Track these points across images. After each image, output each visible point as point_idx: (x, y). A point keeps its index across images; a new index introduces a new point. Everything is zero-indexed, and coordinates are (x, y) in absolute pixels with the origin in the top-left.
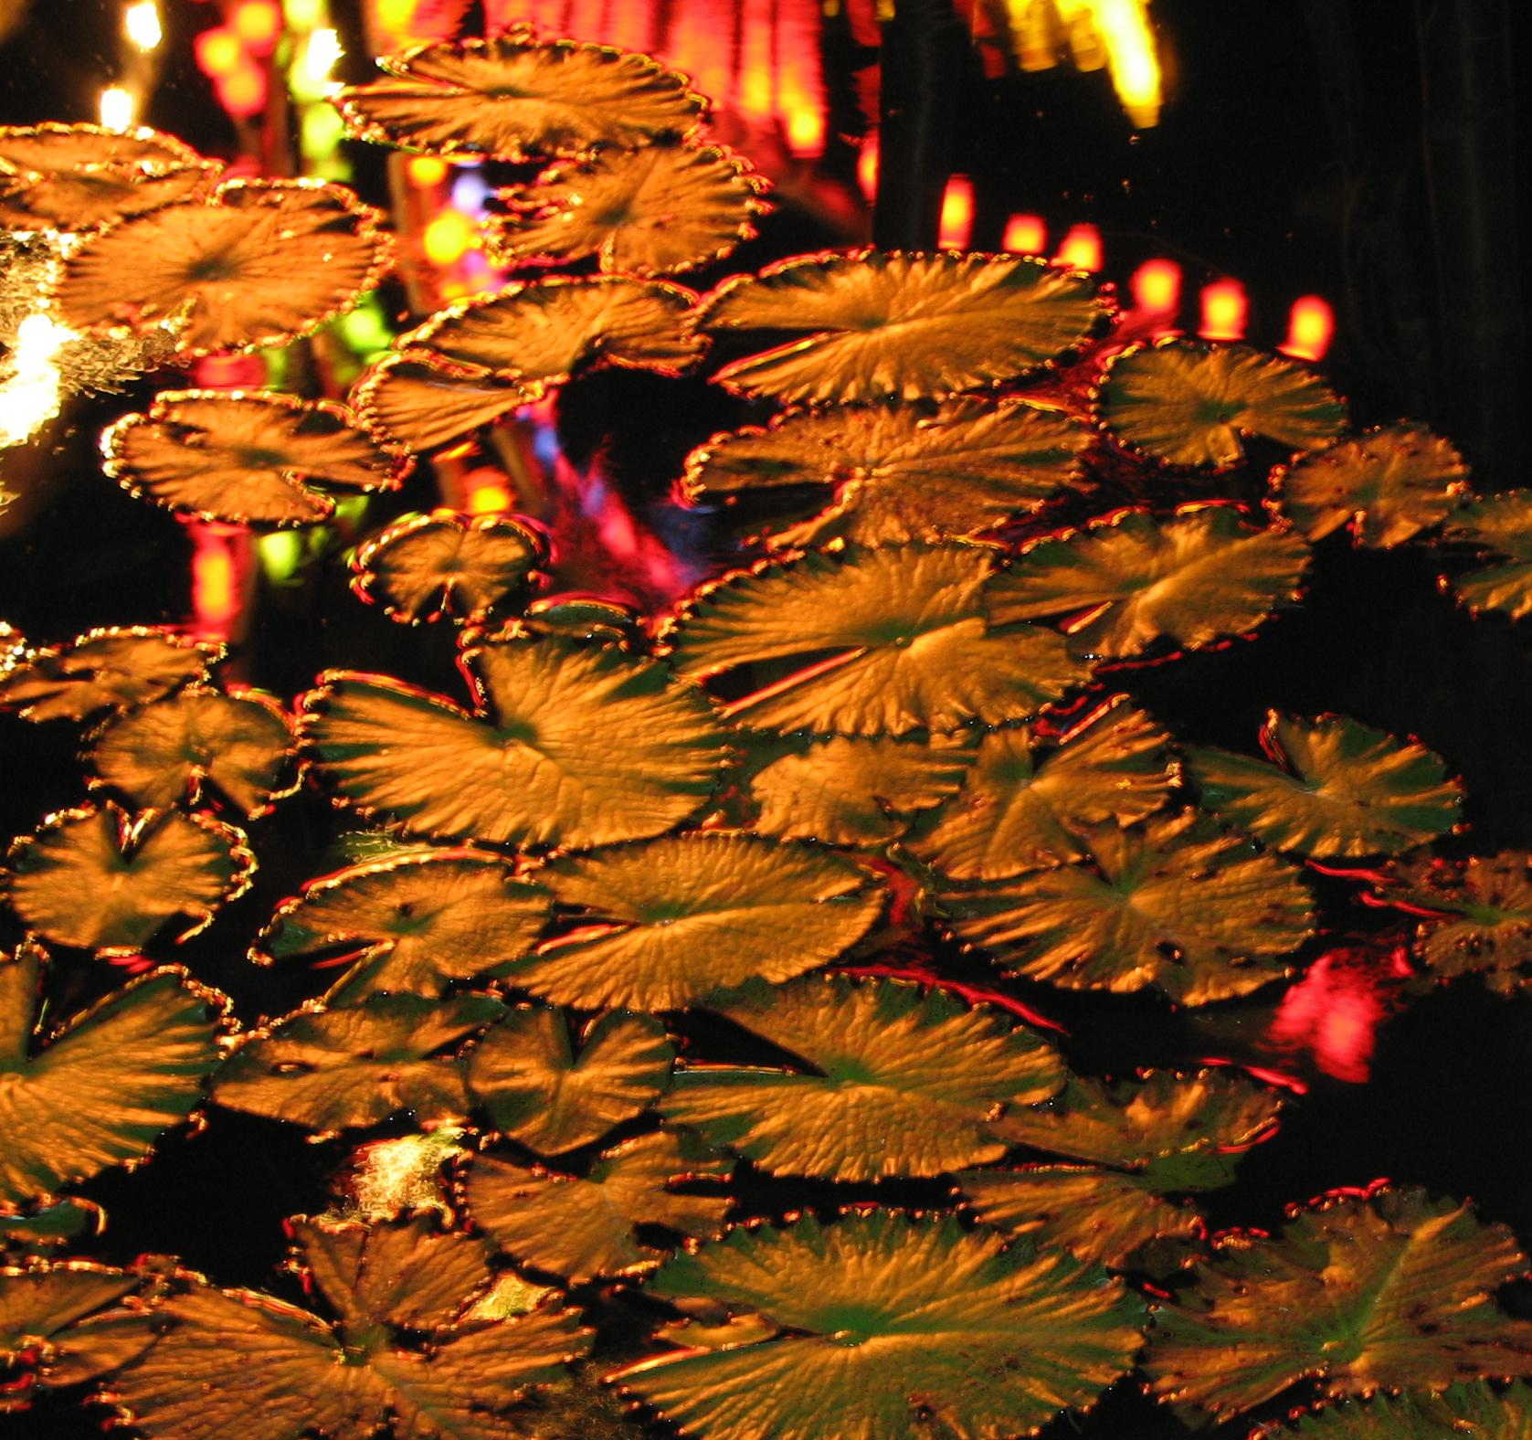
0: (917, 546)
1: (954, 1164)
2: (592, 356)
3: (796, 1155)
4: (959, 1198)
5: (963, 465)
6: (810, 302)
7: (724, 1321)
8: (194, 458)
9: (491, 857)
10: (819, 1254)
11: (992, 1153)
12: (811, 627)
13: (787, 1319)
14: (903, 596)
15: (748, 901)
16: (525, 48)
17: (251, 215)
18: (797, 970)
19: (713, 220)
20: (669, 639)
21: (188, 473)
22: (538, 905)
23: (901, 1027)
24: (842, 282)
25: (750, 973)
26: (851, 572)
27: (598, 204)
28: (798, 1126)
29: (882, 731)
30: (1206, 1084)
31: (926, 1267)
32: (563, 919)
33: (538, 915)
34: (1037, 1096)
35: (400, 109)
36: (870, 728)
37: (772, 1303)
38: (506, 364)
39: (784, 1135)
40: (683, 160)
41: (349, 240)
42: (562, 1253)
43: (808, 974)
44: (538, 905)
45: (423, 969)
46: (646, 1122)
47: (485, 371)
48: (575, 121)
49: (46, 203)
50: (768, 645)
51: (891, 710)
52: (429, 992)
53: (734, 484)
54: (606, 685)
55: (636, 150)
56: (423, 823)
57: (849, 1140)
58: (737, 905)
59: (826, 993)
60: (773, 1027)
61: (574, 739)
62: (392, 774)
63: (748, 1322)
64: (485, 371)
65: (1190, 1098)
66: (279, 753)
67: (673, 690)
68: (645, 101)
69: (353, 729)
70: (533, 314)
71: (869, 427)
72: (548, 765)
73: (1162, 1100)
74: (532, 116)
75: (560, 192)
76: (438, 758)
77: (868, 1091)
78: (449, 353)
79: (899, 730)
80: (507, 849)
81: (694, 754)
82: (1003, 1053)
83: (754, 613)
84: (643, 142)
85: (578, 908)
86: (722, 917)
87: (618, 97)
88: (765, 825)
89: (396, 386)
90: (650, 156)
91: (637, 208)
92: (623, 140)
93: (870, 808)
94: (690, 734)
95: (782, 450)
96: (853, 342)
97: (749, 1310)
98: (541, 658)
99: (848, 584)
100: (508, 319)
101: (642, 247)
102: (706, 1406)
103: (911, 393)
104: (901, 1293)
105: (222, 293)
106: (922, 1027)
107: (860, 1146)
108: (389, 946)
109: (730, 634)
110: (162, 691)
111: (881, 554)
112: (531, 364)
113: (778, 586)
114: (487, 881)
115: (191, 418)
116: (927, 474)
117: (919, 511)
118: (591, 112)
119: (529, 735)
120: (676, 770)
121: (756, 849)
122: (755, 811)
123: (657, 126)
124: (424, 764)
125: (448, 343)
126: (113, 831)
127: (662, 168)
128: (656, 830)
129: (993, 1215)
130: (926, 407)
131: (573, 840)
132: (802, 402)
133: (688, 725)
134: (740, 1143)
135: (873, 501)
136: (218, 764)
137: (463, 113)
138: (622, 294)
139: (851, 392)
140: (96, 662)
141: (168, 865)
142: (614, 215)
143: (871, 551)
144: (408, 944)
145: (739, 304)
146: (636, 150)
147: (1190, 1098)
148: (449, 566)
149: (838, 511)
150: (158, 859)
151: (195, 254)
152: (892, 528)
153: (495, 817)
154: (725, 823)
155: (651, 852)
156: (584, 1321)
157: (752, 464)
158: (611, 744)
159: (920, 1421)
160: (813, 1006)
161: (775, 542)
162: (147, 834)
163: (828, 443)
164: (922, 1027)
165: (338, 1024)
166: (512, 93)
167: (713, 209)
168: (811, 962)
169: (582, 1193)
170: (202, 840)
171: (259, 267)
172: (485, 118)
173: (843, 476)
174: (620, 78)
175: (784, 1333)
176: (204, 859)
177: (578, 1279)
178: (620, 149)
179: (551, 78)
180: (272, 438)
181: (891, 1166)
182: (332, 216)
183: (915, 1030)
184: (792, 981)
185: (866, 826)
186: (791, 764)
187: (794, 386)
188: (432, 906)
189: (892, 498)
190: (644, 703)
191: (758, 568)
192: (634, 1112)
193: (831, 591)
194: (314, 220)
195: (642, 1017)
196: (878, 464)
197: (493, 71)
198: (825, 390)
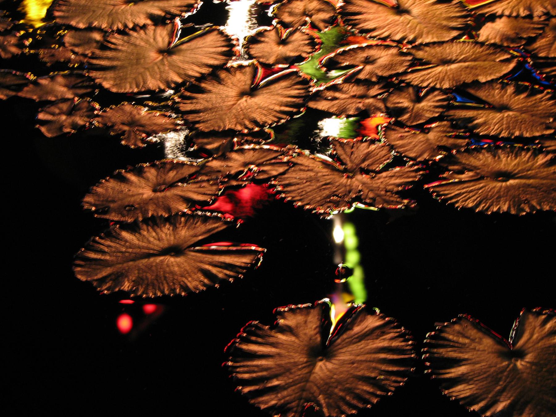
18: (489, 79)
22: (409, 58)
28: (490, 122)
31: (528, 162)
32: (418, 64)
36: (514, 14)
39: (484, 123)
46: (440, 118)
51: (521, 10)
56: (374, 34)
57: (504, 126)
60: (482, 94)
81: (460, 20)
94: (458, 14)
107: (508, 128)
114: (394, 51)
121: (478, 46)
122: (478, 36)
128: (447, 39)
168: (493, 77)
181: (517, 133)
185: (513, 40)
186: (489, 25)
192: (437, 115)
195: (440, 89)
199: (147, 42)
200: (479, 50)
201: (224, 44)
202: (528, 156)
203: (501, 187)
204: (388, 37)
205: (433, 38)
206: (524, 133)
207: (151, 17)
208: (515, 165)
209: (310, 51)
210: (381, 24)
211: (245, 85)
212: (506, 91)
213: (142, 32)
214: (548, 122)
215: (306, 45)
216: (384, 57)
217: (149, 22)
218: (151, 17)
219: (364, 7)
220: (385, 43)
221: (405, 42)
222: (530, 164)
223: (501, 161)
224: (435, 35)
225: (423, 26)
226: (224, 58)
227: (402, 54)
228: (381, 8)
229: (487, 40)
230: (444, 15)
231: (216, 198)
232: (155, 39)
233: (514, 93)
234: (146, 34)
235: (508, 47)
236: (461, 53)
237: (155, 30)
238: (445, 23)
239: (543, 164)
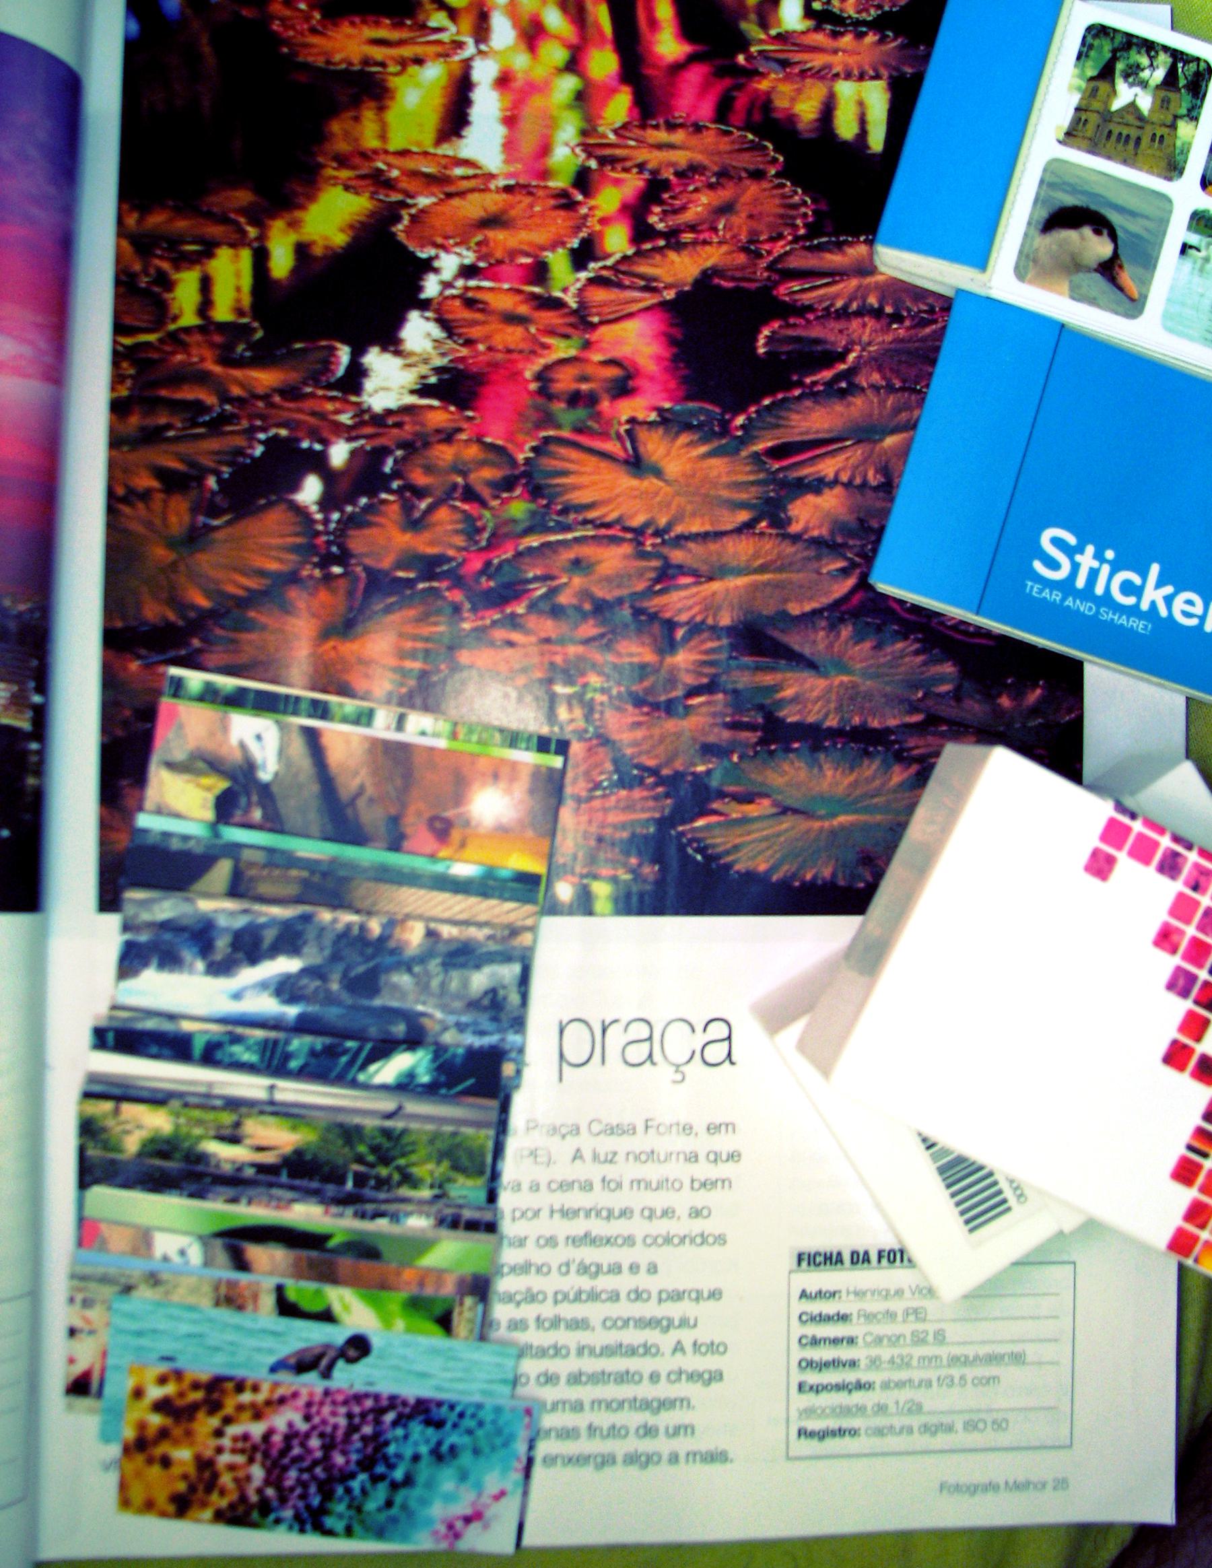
0: (890, 388)
1: (892, 722)
2: (706, 278)
3: (799, 712)
4: (896, 742)
5: (917, 349)
6: (834, 259)
7: (751, 801)
8: (478, 316)
9: (629, 536)
10: (811, 767)
11: (917, 718)
12: (826, 426)
13: (789, 802)
14: (880, 414)
15: (780, 570)
16: (681, 126)
17: (518, 198)
18: (808, 608)
19: (782, 216)
20: (743, 427)
21: (473, 323)
22: (655, 563)
23: (867, 645)
24: (851, 251)
25: (781, 608)
26: (850, 399)
27: (716, 203)
28: (806, 695)
29: (864, 484)
30: (1043, 688)
31: (874, 778)
32: (667, 575)
33: (655, 569)
34: (944, 688)
35: (608, 152)
36: (858, 481)
37: (781, 793)
38: (655, 279)
39: (795, 699)
40: (765, 185)
41: (572, 214)
42: (656, 757)
43: (815, 613)
44: (655, 563)
45: (586, 594)
46: (710, 688)
47: (642, 283)
48: (706, 162)
49: (403, 185)
50: (801, 434)
51: (871, 474)
52: (587, 607)
53: (785, 348)
54: (703, 449)
55: (740, 179)
56: (592, 515)
57: (832, 706)
58: (774, 571)
59: (823, 623)
60: (795, 641)
61: (684, 475)
62: (575, 488)
63: (766, 802)
64: (642, 283)
65: (1034, 696)
66: (508, 472)
67: (744, 454)
68: (746, 156)
69: (554, 462)
70: (673, 255)
71: (864, 325)
72: (668, 489)
73: (1018, 696)
74: (681, 158)
75: (695, 196)
76: (603, 481)
77: (845, 679)
78: (624, 273)
79: (874, 483)
80: (639, 532)
81: (753, 489)
82: (925, 664)
83: (795, 417)
84: (744, 175)
85: (680, 567)
86: (766, 577)
87: (731, 152)
88: (795, 528)
89: (590, 288)
90: (748, 182)
91: (738, 207)
92: (732, 173)
93: (854, 525)
94: (752, 478)
95: (816, 332)
96: (854, 282)
97: (767, 796)
98: (667, 432)
99: (849, 405)
100: (658, 258)
101: (740, 227)
102: (736, 848)
103: (889, 310)
104: (858, 792)
105: (498, 235)
106: (878, 647)
107: (839, 709)
108: (564, 580)
109: (778, 426)
110: (443, 436)
111: (869, 392)
112: (669, 280)
113: (808, 403)
114: (627, 549)
115: (479, 296)
116: (897, 352)
117: (891, 369)
118: (716, 159)
119: (658, 473)
120: (744, 496)
121: (787, 542)
122: (789, 521)
123: (751, 167)
124: (594, 483)
125: (623, 268)
126: (408, 508)
127: (753, 189)
128: (729, 527)
129: (916, 752)
130: (897, 318)
131: (679, 529)
132: (827, 309)
133: (750, 473)
134: (767, 702)
135: (866, 363)
136: (472, 476)
137: (642, 155)
138: (724, 248)
139: (854, 306)
140: (407, 419)
141: (439, 529)
142: (726, 209)
143: (863, 390)
144: (577, 581)
145: (791, 258)
146: (740, 179)
147: (1034, 696)
148: (584, 379)
149: (843, 367)
150: (435, 525)
151: (483, 214)
152: (876, 377)
153: (636, 514)
154: (770, 526)
155: (725, 540)
156: (667, 796)
157: (798, 339)
158: (705, 480)
159: (864, 864)
160: (816, 631)
161: (808, 381)
162: (430, 509)
163: (841, 331)
164: (878, 647)
165: (532, 622)
166: (671, 146)
167: (781, 211)
168: (815, 605)
169: (671, 725)
170: (459, 516)
171: (520, 223)
172: (654, 158)
173: (847, 351)
174: (733, 142)
175: (785, 810)
176: (460, 526)
177: (666, 772)
178: (731, 178)
179: (694, 141)
180: (523, 309)
181: (856, 720)
182: (563, 201)
183: (874, 648)
184: (804, 615)
185: (850, 534)
186: (811, 499)
187: (820, 302)
188: (593, 560)
189: (877, 361)
190: (725, 460)
191: (797, 393)
192: (705, 680)
193: (839, 408)
194: (552, 202)
195: (713, 628)
196: (869, 344)
197: (662, 136)
198: (839, 304)
199: (149, 525)
200: (789, 549)
201: (292, 529)
202: (874, 767)
203: (821, 829)
204: (619, 520)
205: (703, 524)
206: (870, 720)
207: (162, 474)
208: (850, 785)
209: (463, 544)
210: (606, 495)
211: (705, 562)
212: (838, 635)
213: (141, 505)
214: (914, 698)
215: (457, 532)
216: (612, 558)
217: (155, 484)
218: (162, 474)
219: (572, 461)
220: (610, 531)
221: (650, 531)
222: (877, 782)
223: (824, 776)
224: (707, 518)
225: (682, 500)
226: (293, 557)
227: (642, 555)
228: (603, 464)
229: (806, 530)
230: (724, 479)
231: (348, 1491)
232: (165, 519)
233: (851, 638)
234: (148, 508)
235: (844, 545)
236: (756, 556)
237: (165, 502)
238: (725, 494)
239: (901, 785)
